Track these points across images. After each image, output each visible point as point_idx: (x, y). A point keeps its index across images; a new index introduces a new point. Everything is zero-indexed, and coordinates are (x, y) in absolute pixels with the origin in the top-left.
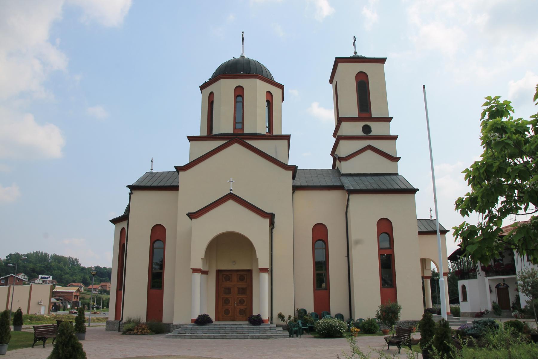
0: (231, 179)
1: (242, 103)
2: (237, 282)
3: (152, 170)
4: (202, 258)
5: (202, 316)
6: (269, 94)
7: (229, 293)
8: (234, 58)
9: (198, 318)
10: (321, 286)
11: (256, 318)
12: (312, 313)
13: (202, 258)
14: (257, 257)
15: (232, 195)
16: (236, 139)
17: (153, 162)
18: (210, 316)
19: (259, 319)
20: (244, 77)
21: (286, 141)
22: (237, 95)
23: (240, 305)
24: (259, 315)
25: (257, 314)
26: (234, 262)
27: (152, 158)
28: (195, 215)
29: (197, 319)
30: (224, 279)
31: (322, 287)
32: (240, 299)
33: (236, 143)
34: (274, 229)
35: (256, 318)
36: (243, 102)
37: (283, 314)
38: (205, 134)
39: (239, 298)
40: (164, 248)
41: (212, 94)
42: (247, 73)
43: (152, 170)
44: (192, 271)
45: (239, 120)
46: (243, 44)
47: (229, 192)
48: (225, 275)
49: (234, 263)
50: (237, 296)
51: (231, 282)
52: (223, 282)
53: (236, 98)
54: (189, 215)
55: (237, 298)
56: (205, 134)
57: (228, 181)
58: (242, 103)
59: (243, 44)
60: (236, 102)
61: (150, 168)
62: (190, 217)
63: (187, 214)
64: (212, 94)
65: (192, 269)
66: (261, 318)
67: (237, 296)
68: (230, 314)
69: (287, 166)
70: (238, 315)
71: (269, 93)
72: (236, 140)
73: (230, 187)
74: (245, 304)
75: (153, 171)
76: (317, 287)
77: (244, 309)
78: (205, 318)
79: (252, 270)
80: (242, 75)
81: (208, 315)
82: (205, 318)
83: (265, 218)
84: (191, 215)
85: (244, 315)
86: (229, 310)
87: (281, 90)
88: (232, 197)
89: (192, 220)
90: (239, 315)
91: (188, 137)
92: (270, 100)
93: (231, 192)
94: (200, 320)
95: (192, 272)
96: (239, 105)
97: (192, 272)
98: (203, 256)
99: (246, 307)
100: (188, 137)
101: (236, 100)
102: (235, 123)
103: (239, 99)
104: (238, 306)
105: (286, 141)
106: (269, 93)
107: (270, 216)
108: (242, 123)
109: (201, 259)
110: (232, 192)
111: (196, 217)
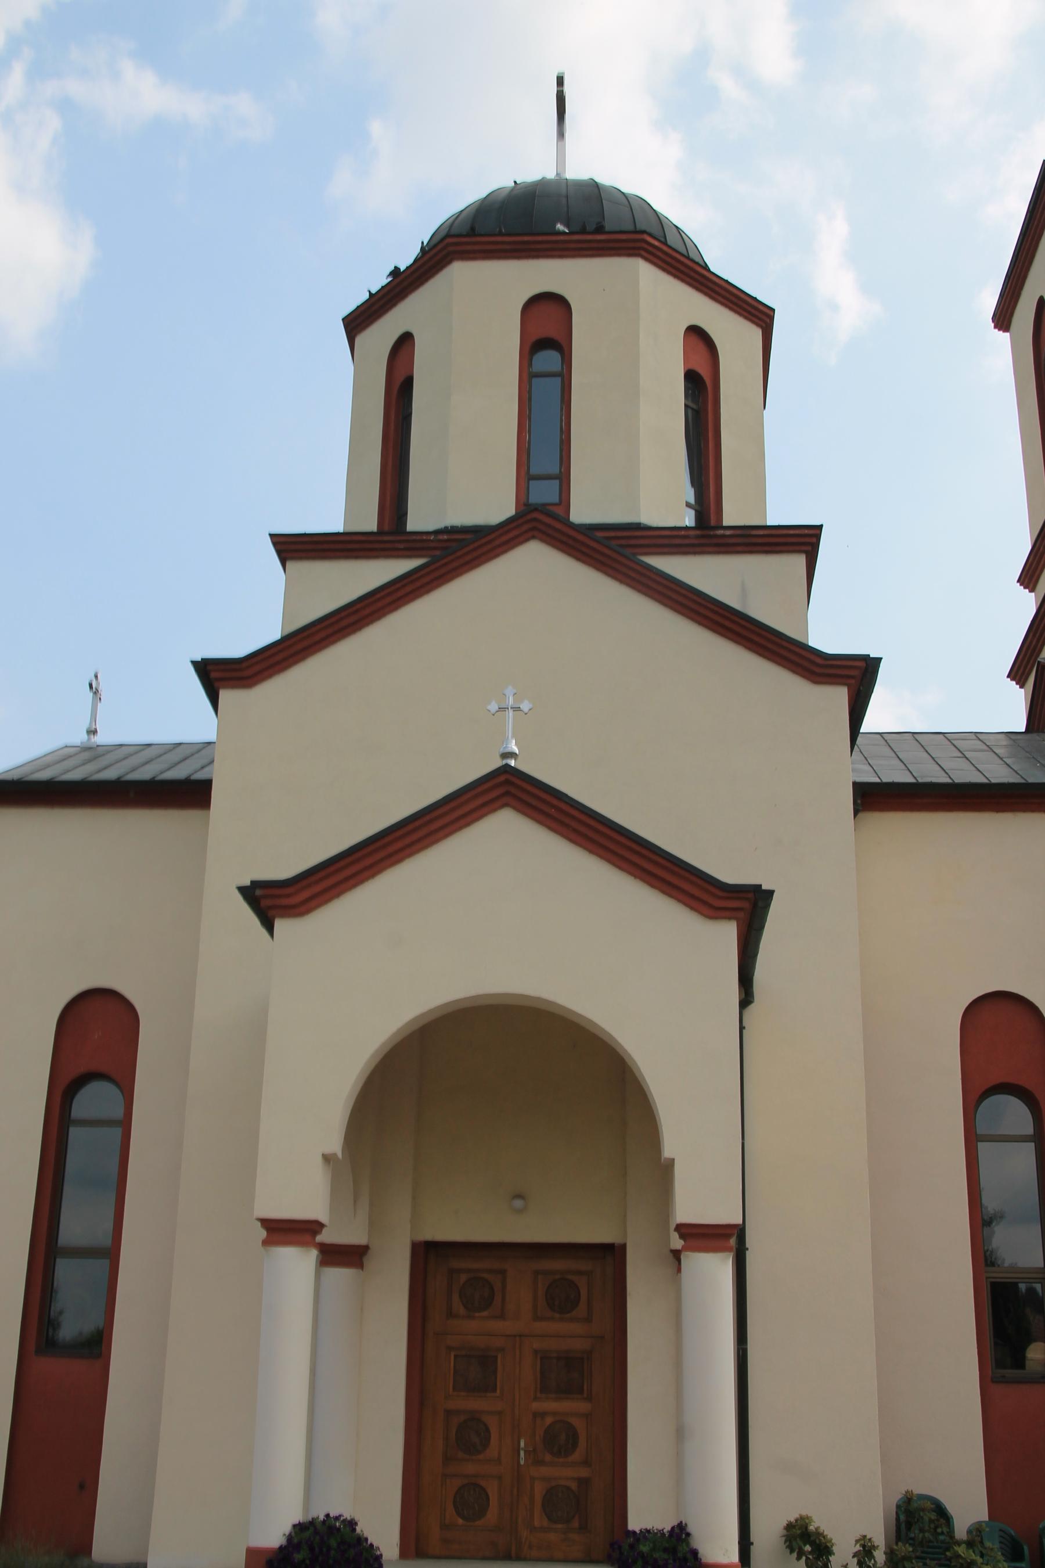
0: (510, 691)
1: (558, 380)
2: (537, 1318)
3: (93, 732)
4: (327, 1158)
5: (316, 1532)
6: (694, 339)
7: (486, 1386)
8: (515, 182)
9: (290, 1538)
10: (1019, 1362)
11: (666, 1550)
12: (980, 1523)
13: (327, 1158)
14: (1026, 605)
15: (513, 779)
16: (535, 515)
17: (104, 693)
18: (364, 1528)
19: (685, 1559)
20: (574, 249)
21: (799, 561)
22: (534, 338)
23: (548, 1457)
24: (680, 1533)
25: (666, 1524)
26: (520, 1196)
27: (96, 677)
28: (288, 896)
29: (281, 1548)
30: (456, 1297)
31: (1027, 1362)
32: (549, 1420)
33: (533, 537)
34: (752, 1005)
35: (666, 1550)
36: (565, 377)
37: (820, 1522)
38: (371, 525)
39: (543, 1415)
40: (125, 1123)
41: (405, 342)
42: (590, 227)
43: (93, 732)
44: (264, 1233)
45: (545, 462)
46: (561, 134)
47: (498, 763)
48: (463, 1278)
49: (518, 1203)
50: (536, 1406)
51: (502, 1316)
52: (451, 1314)
53: (531, 360)
54: (258, 892)
55: (987, 1278)
56: (371, 525)
57: (493, 707)
58: (558, 380)
59: (561, 134)
60: (528, 377)
61: (85, 724)
62: (264, 903)
63: (242, 890)
64: (405, 342)
65: (267, 1223)
66: (695, 1553)
67: (536, 1406)
68: (492, 1515)
69: (819, 661)
70: (537, 1523)
71: (697, 334)
72: (535, 520)
73: (505, 740)
74: (577, 1456)
75: (100, 739)
76: (999, 1364)
77: (574, 1486)
78: (333, 1543)
79: (623, 1247)
80: (562, 238)
81: (352, 1524)
82: (333, 1543)
83: (711, 917)
84: (266, 897)
85: (576, 1524)
86: (483, 1489)
87: (757, 333)
88: (513, 790)
89: (269, 927)
90: (545, 1523)
91: (276, 539)
92: (705, 372)
93: (507, 765)
94: (298, 1557)
95: (266, 1243)
96: (547, 389)
97: (266, 1243)
98: (335, 1144)
99: (584, 1472)
100: (276, 539)
101: (530, 365)
102: (525, 476)
103: (548, 359)
104: (539, 1462)
105: (800, 561)
106: (697, 334)
107: (746, 905)
108: (564, 478)
109: (320, 1159)
110: (512, 763)
111: (299, 909)
